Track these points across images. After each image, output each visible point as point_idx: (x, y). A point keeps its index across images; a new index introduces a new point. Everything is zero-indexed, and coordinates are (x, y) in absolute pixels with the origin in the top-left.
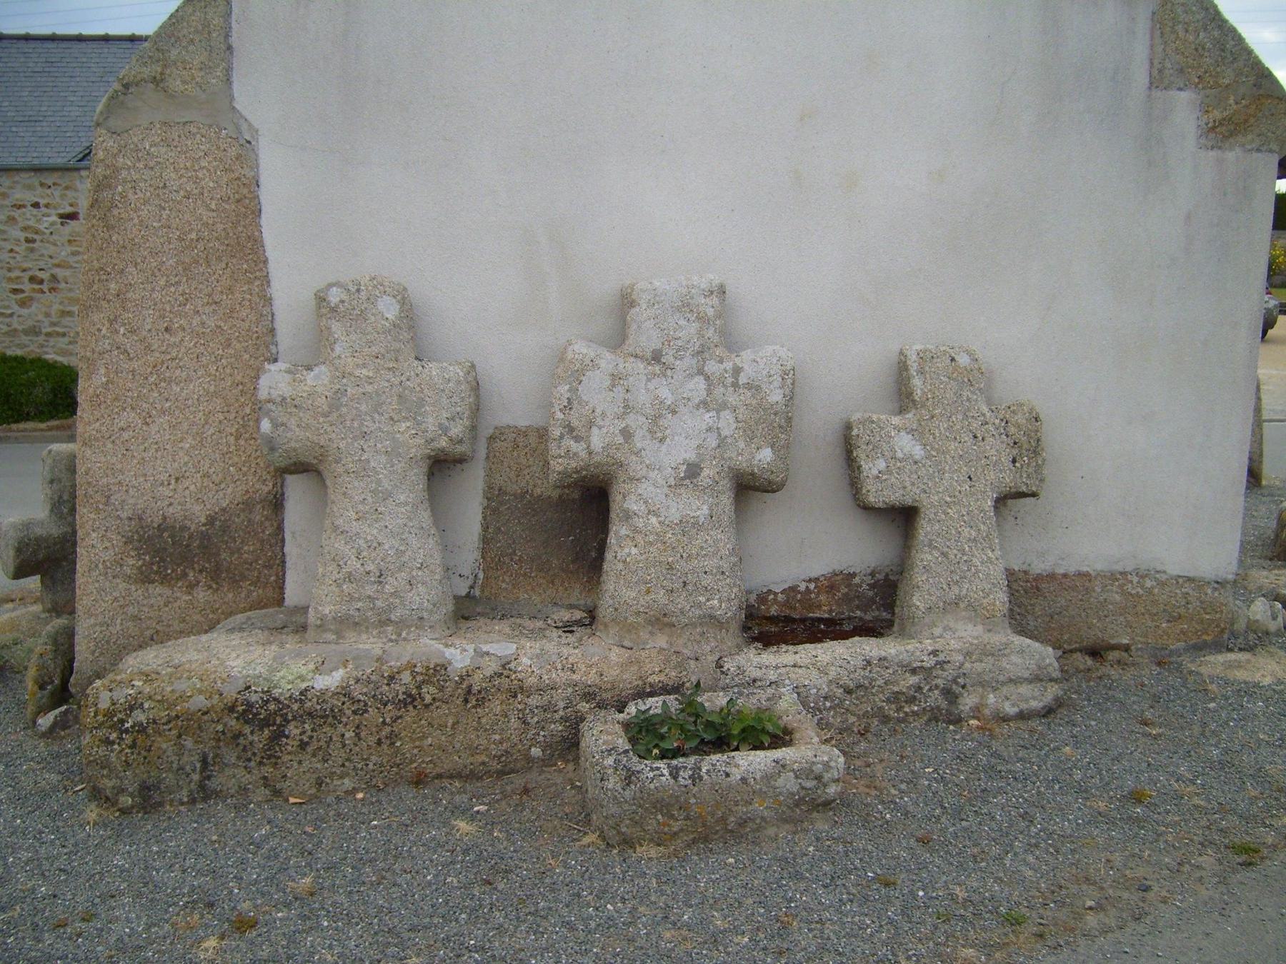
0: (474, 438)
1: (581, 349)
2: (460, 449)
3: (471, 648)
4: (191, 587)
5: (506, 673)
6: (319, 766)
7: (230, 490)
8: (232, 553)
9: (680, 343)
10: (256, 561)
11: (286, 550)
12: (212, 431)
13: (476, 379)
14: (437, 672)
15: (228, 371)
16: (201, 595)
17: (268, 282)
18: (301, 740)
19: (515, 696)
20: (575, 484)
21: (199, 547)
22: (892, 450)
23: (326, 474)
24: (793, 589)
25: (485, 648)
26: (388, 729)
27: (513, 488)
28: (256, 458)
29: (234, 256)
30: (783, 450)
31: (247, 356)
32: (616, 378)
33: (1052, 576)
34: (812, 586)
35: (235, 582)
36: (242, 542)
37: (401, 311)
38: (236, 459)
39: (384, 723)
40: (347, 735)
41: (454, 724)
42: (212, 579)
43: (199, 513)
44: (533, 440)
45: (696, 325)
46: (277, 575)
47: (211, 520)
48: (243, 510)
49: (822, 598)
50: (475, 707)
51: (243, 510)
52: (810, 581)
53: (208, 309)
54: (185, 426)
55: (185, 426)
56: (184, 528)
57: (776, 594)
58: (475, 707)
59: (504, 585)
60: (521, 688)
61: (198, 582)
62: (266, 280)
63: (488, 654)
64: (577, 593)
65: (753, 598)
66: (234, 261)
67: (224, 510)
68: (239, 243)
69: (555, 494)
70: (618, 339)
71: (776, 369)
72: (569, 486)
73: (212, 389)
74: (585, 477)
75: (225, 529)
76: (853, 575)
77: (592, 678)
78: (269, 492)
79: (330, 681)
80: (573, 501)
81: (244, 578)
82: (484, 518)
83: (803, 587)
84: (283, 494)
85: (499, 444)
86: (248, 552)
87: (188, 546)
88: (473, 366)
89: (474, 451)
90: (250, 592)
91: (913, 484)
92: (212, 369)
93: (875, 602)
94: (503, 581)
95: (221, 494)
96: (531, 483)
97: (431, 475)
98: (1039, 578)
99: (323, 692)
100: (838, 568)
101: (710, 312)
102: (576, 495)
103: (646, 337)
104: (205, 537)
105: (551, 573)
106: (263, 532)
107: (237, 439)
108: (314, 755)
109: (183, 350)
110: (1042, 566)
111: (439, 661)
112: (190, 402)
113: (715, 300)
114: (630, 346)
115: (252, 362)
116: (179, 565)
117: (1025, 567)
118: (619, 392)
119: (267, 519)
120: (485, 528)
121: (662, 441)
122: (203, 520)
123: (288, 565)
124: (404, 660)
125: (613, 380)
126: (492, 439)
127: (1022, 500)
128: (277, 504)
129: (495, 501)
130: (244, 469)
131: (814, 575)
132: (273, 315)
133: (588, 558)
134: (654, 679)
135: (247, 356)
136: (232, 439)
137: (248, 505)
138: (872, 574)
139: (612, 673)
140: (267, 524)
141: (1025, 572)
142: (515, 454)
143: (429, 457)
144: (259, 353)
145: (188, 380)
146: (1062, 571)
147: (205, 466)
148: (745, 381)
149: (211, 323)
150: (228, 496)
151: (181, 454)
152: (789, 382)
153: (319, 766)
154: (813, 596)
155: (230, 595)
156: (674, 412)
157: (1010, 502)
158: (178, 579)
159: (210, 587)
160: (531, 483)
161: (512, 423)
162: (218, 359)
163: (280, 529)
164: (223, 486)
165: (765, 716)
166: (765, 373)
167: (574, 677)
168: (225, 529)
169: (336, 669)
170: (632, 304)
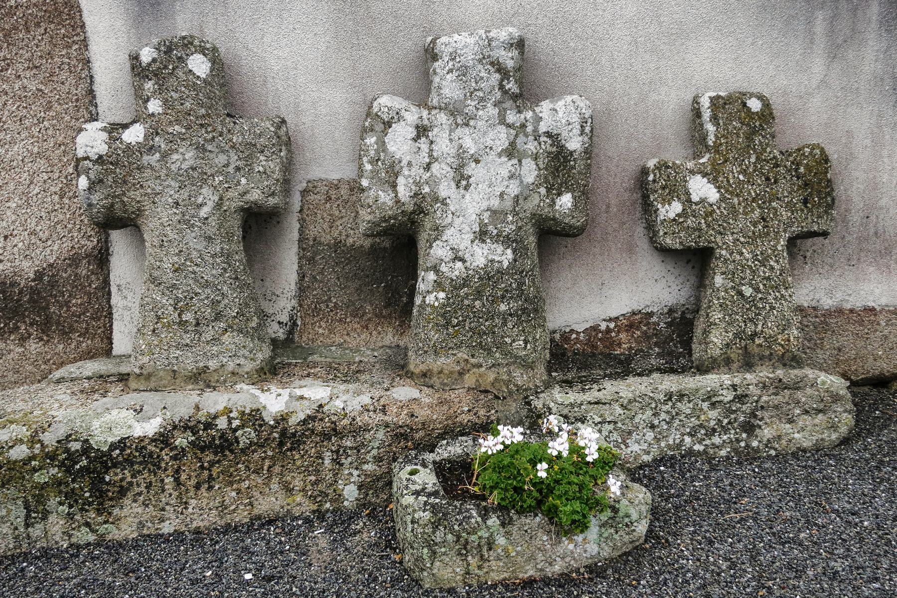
0: (287, 191)
1: (386, 102)
2: (272, 201)
3: (285, 396)
4: (23, 339)
5: (320, 416)
6: (140, 510)
7: (56, 248)
8: (61, 307)
9: (481, 94)
10: (84, 314)
11: (113, 301)
12: (37, 190)
13: (287, 133)
14: (254, 417)
15: (50, 132)
16: (34, 346)
17: (86, 46)
18: (121, 487)
19: (330, 439)
20: (385, 233)
21: (29, 302)
22: (688, 194)
23: (144, 228)
24: (595, 328)
25: (299, 392)
26: (206, 473)
27: (326, 238)
28: (80, 215)
29: (52, 22)
30: (584, 196)
31: (67, 118)
32: (422, 131)
33: (840, 311)
34: (612, 325)
35: (65, 335)
36: (70, 296)
37: (212, 70)
38: (61, 217)
39: (202, 467)
40: (166, 481)
41: (270, 467)
42: (43, 332)
43: (29, 269)
44: (344, 191)
45: (498, 76)
46: (105, 326)
47: (39, 276)
48: (70, 265)
49: (623, 336)
50: (290, 450)
51: (70, 265)
52: (610, 320)
53: (28, 74)
54: (11, 186)
55: (11, 186)
56: (13, 284)
57: (578, 333)
58: (290, 450)
59: (321, 331)
60: (335, 430)
61: (30, 335)
62: (85, 44)
63: (302, 397)
64: (390, 336)
65: (557, 336)
66: (52, 26)
67: (51, 265)
68: (56, 9)
69: (367, 243)
70: (421, 90)
71: (575, 119)
72: (379, 234)
73: (36, 150)
74: (393, 225)
75: (53, 284)
76: (651, 314)
77: (403, 418)
78: (93, 248)
79: (150, 427)
80: (385, 249)
81: (72, 330)
82: (301, 267)
83: (603, 326)
84: (107, 249)
85: (311, 197)
86: (76, 305)
87: (18, 301)
88: (283, 121)
89: (287, 203)
90: (79, 343)
91: (708, 226)
92: (35, 130)
93: (672, 340)
94: (320, 327)
95: (48, 250)
96: (344, 233)
97: (246, 228)
98: (829, 313)
99: (141, 439)
100: (636, 307)
101: (510, 64)
102: (387, 244)
103: (448, 87)
104: (33, 291)
105: (365, 318)
106: (90, 285)
107: (61, 197)
108: (135, 501)
109: (6, 113)
110: (830, 302)
111: (254, 407)
112: (15, 164)
113: (515, 53)
114: (435, 101)
115: (72, 123)
116: (10, 319)
117: (814, 304)
118: (423, 143)
119: (93, 273)
120: (302, 277)
121: (466, 188)
122: (32, 276)
123: (115, 316)
124: (220, 407)
125: (418, 132)
126: (305, 193)
127: (810, 241)
128: (102, 258)
129: (309, 252)
130: (70, 226)
131: (614, 314)
132: (92, 77)
133: (398, 304)
134: (465, 418)
135: (67, 118)
136: (56, 198)
137: (74, 260)
138: (671, 311)
139: (423, 414)
140: (93, 277)
141: (815, 309)
142: (328, 205)
143: (242, 209)
144: (80, 114)
145: (13, 142)
146: (848, 306)
147: (32, 223)
148: (545, 130)
149: (32, 86)
150: (54, 251)
151: (9, 213)
152: (588, 129)
153: (140, 510)
154: (613, 334)
155: (61, 346)
156: (477, 161)
157: (798, 241)
158: (11, 332)
159: (42, 340)
160: (344, 233)
161: (323, 176)
162: (41, 121)
163: (106, 282)
164: (49, 243)
165: (401, 330)
166: (564, 121)
167: (386, 418)
168: (53, 284)
169: (154, 416)
170: (435, 57)
